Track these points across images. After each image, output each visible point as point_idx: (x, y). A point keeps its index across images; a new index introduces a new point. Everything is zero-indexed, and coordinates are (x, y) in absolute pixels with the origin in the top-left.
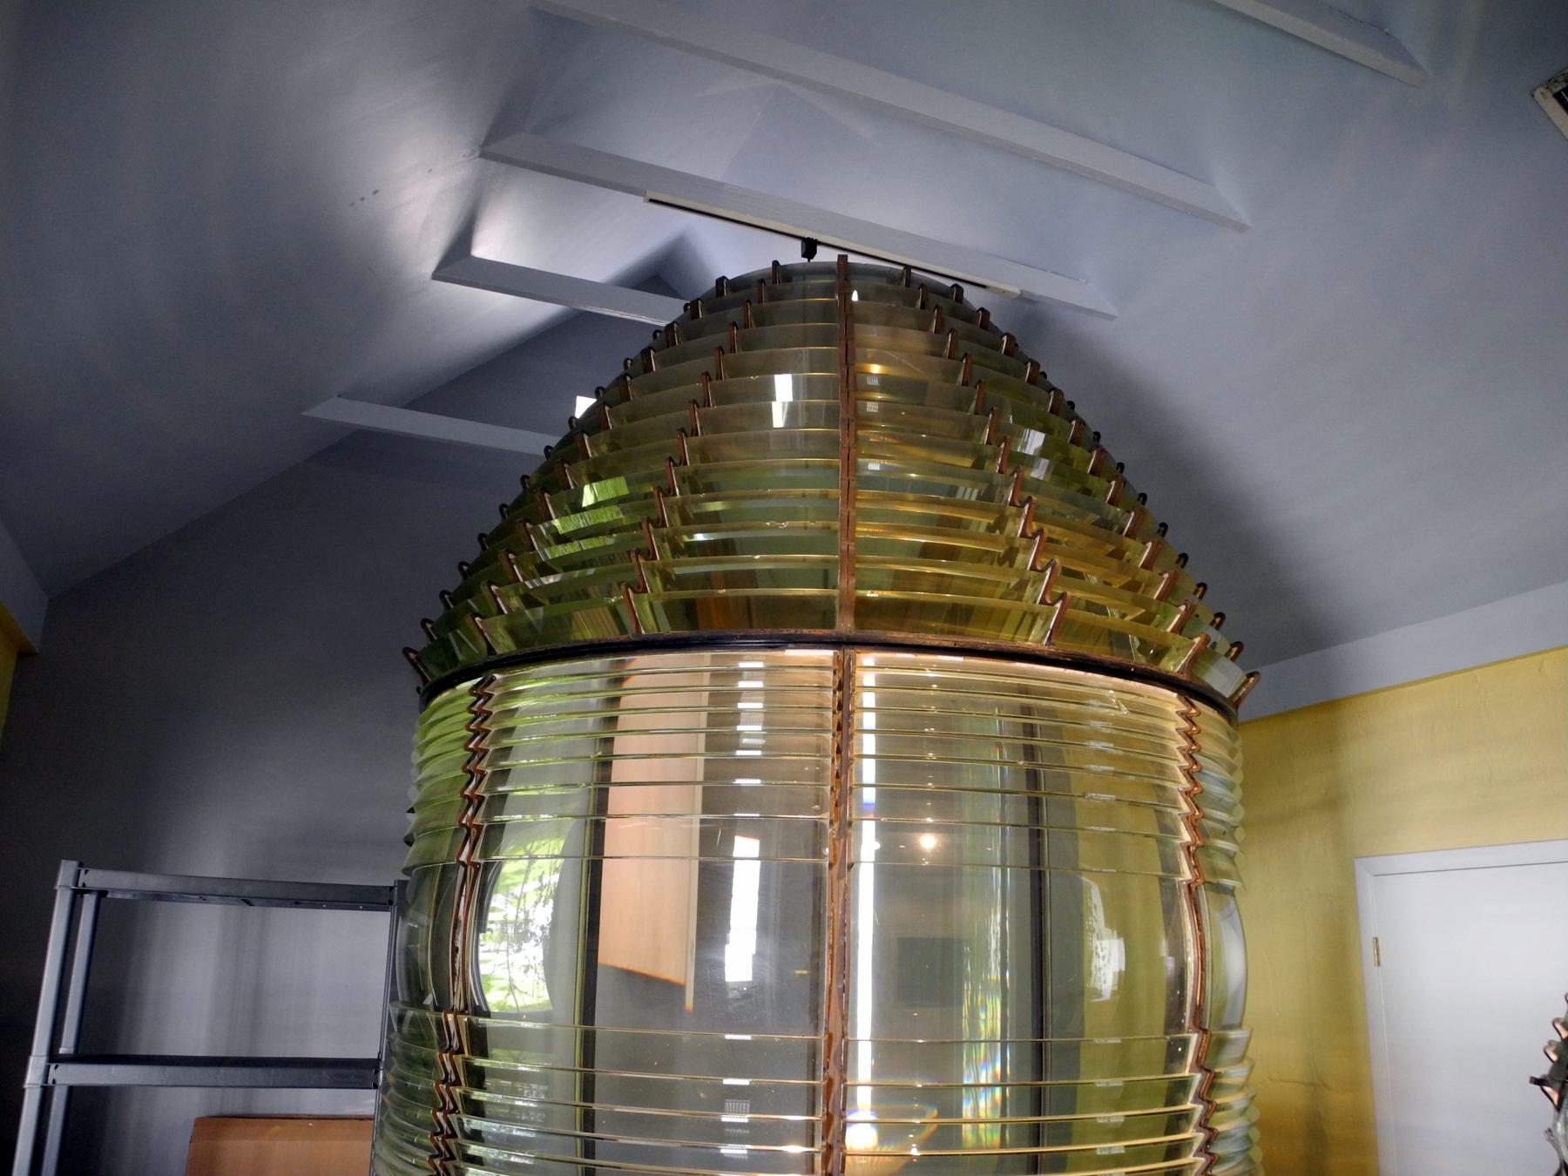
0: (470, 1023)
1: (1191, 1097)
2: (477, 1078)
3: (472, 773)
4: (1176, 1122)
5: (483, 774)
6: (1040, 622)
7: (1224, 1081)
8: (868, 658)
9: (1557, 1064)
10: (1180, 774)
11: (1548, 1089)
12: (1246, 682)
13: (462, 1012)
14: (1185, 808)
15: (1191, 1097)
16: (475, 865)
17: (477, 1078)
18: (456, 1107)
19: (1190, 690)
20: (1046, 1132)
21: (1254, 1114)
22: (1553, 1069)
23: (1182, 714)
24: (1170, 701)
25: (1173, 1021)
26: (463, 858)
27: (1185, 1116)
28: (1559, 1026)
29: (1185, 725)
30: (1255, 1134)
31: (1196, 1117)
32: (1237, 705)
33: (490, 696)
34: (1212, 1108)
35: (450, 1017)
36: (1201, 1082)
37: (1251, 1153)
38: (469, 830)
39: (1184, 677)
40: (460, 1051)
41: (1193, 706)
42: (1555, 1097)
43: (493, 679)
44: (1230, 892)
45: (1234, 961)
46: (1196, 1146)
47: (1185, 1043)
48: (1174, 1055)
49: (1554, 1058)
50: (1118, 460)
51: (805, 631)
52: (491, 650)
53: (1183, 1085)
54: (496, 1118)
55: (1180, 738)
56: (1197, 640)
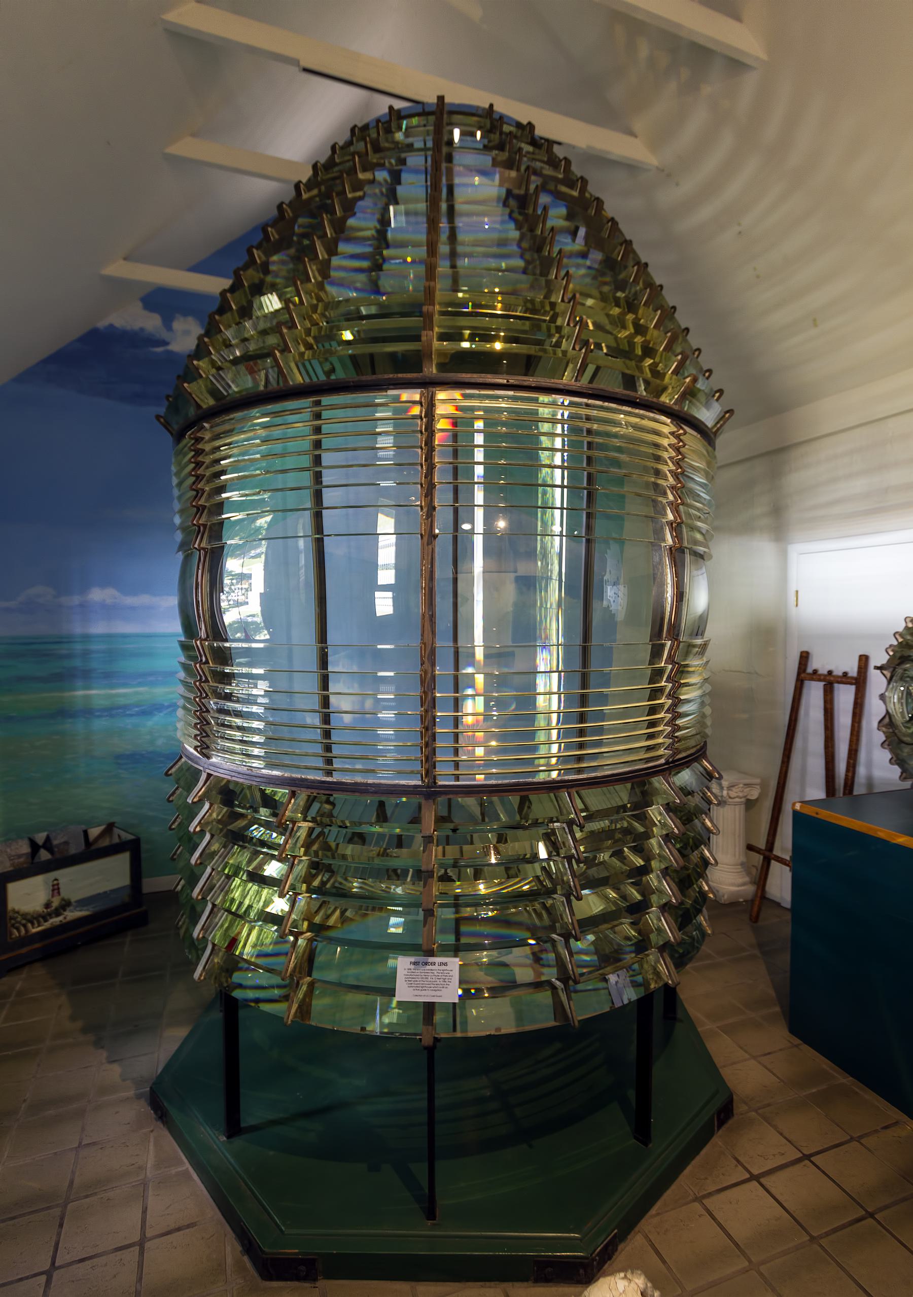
0: (211, 647)
1: (664, 679)
2: (227, 678)
3: (199, 493)
4: (656, 693)
5: (203, 491)
6: (571, 366)
7: (690, 669)
8: (441, 395)
9: (892, 658)
10: (669, 475)
11: (885, 672)
12: (724, 416)
13: (205, 640)
14: (671, 497)
15: (664, 679)
16: (204, 549)
17: (227, 678)
18: (207, 695)
19: (681, 418)
20: (591, 698)
21: (708, 688)
22: (889, 661)
23: (672, 433)
24: (666, 425)
25: (657, 633)
26: (196, 546)
27: (661, 690)
28: (897, 636)
29: (674, 441)
30: (707, 700)
31: (668, 690)
32: (715, 433)
33: (202, 439)
34: (678, 686)
35: (198, 642)
36: (672, 670)
37: (704, 710)
38: (199, 528)
39: (676, 408)
40: (207, 662)
41: (682, 428)
42: (888, 675)
43: (203, 427)
44: (701, 556)
45: (700, 599)
46: (666, 708)
47: (663, 646)
48: (657, 652)
49: (891, 653)
50: (671, 305)
51: (400, 375)
52: (198, 406)
53: (661, 672)
54: (238, 701)
55: (670, 450)
56: (688, 380)
